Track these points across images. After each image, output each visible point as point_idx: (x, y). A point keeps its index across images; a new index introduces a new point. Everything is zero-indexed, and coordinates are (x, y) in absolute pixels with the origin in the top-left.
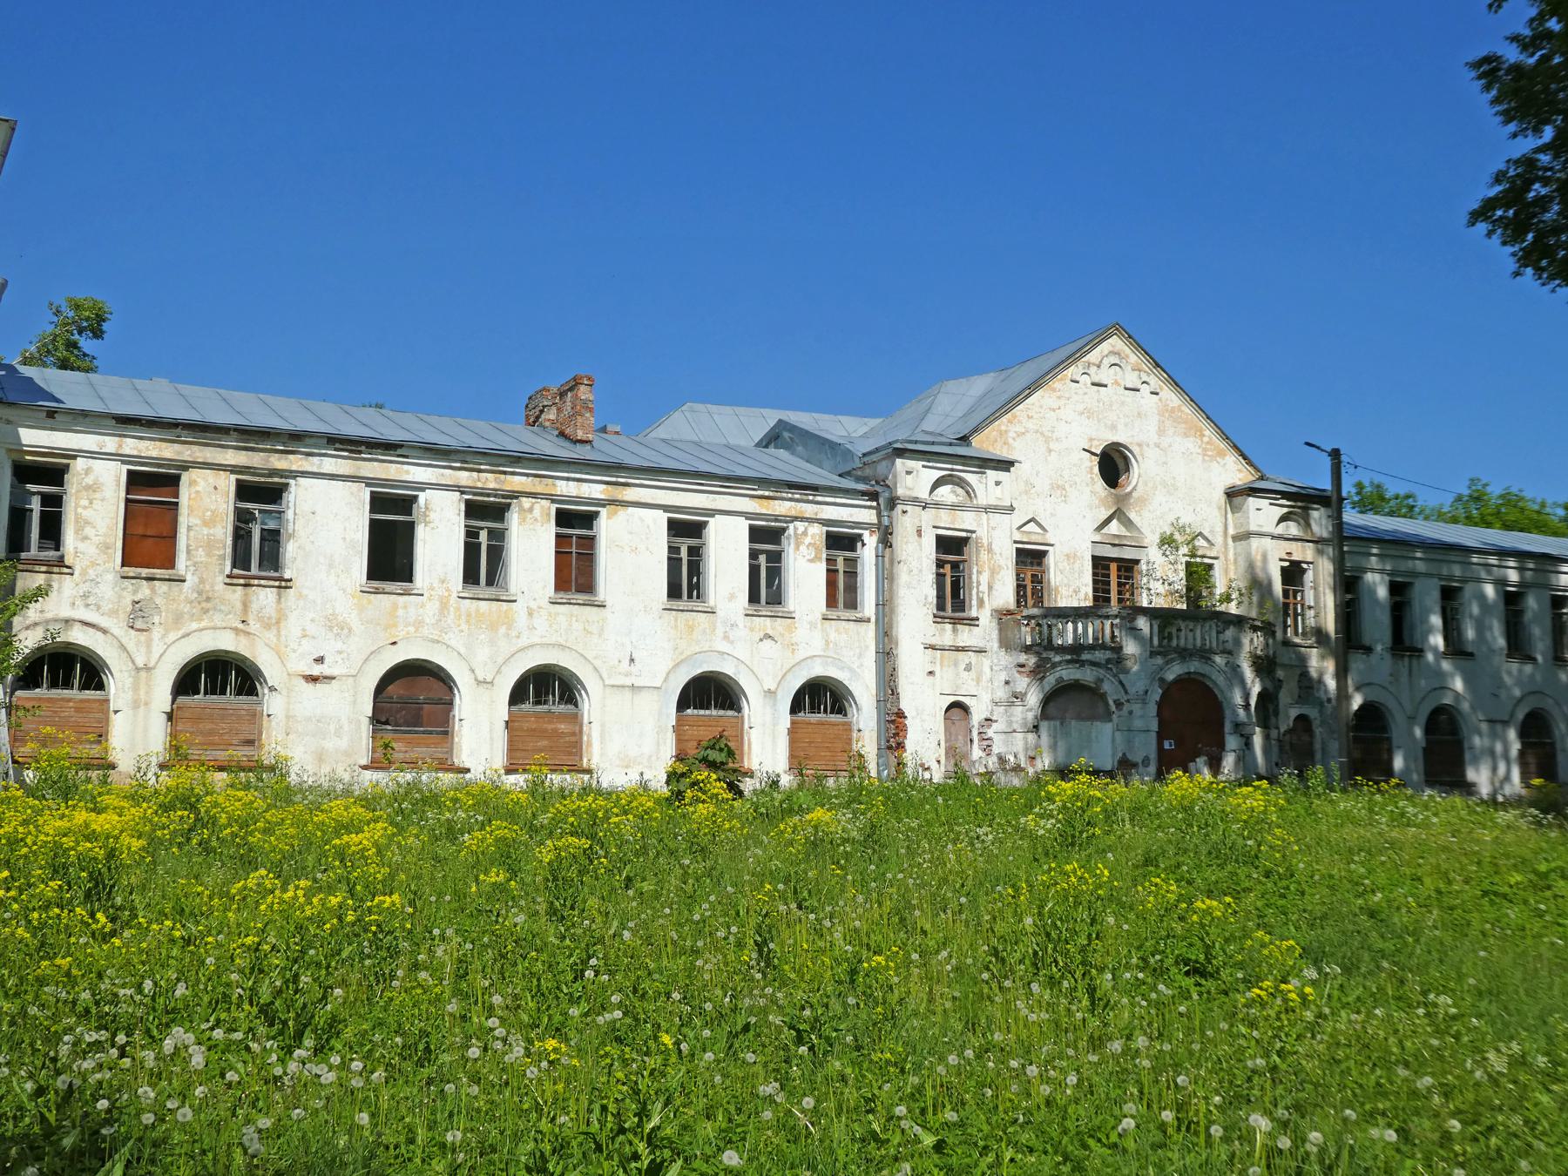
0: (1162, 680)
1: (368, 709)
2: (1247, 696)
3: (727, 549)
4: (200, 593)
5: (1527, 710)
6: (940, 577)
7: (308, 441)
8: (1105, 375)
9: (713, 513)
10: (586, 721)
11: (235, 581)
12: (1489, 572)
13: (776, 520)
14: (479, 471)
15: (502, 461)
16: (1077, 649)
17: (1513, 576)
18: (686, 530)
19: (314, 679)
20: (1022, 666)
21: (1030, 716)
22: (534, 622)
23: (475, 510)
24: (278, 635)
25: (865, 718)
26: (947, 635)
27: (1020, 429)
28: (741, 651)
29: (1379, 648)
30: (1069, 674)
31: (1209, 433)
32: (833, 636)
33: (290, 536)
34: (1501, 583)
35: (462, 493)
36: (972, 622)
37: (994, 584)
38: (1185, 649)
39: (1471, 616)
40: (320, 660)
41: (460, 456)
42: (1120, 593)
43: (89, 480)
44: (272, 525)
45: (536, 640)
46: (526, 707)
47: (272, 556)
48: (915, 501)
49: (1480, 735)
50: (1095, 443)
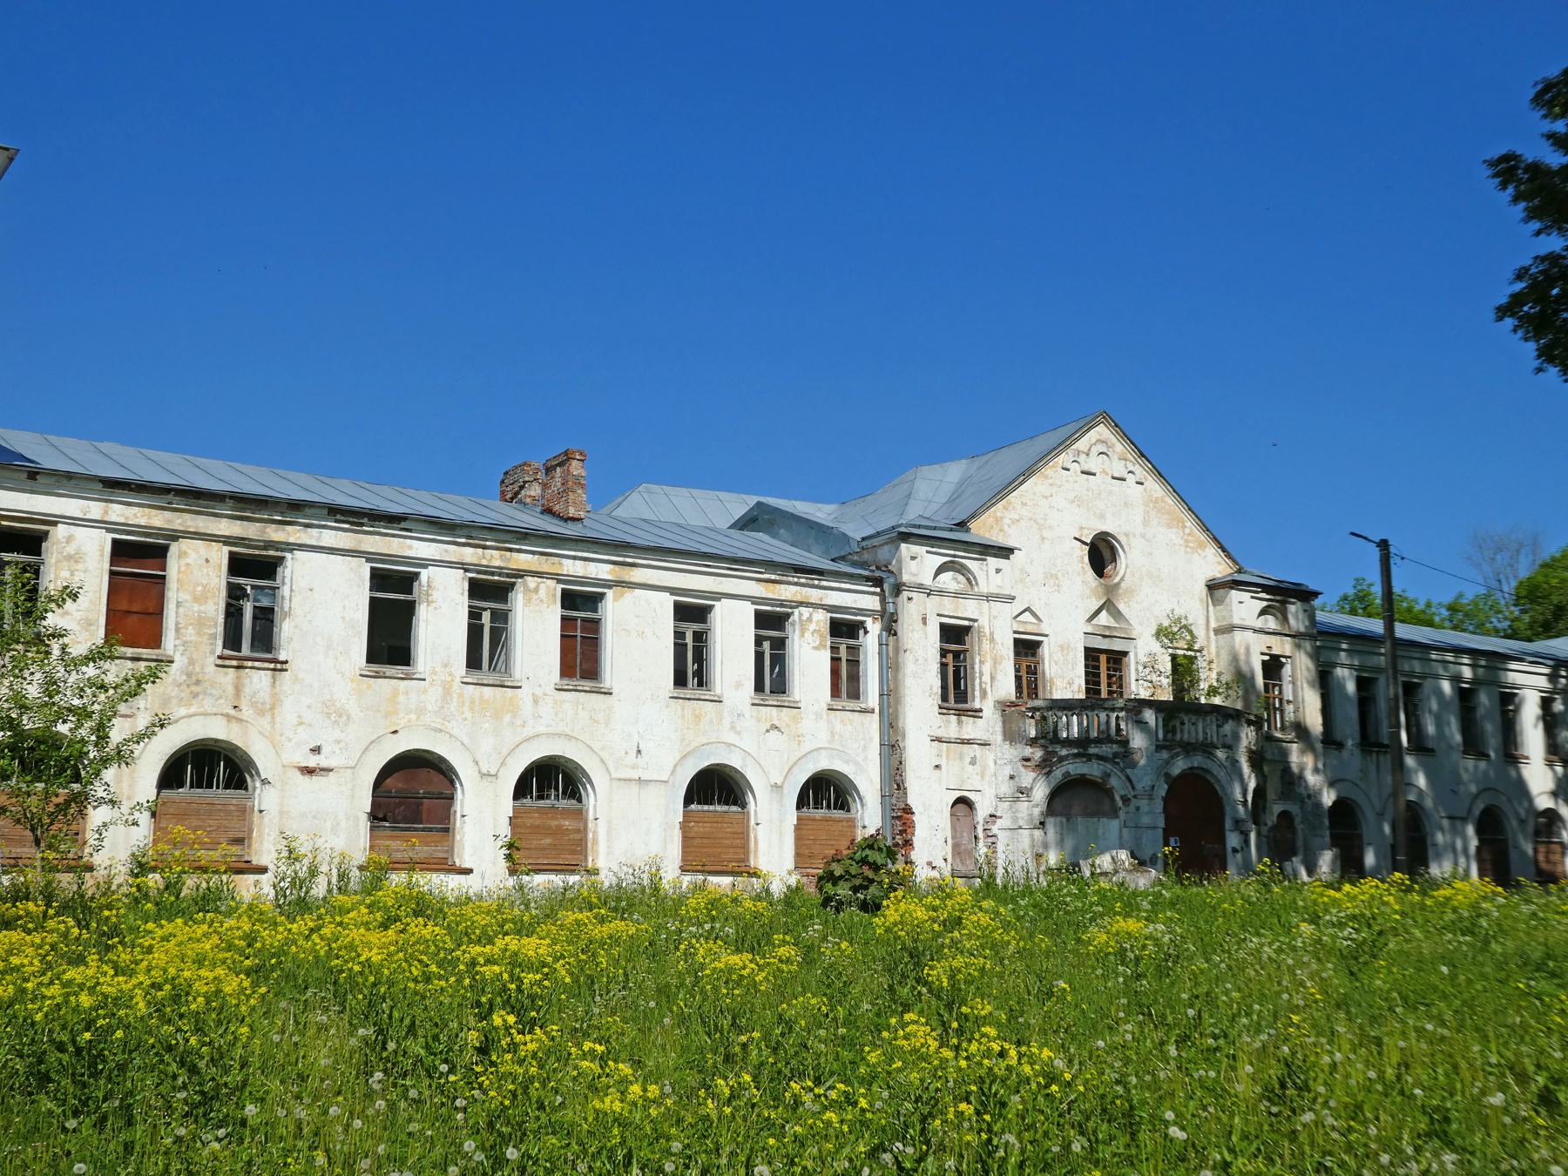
0: (1167, 775)
1: (366, 804)
2: (1245, 794)
3: (733, 634)
4: (189, 675)
5: (1482, 806)
6: (944, 666)
7: (308, 511)
8: (1093, 463)
9: (718, 596)
10: (591, 816)
11: (227, 662)
12: (1446, 669)
13: (782, 606)
14: (485, 547)
15: (508, 537)
16: (1083, 742)
17: (1467, 673)
18: (692, 614)
19: (309, 771)
20: (1027, 760)
21: (1037, 811)
22: (534, 712)
23: (479, 590)
24: (273, 722)
25: (869, 817)
26: (951, 726)
27: (1014, 516)
28: (747, 743)
29: (1350, 743)
30: (1076, 768)
31: (1190, 524)
32: (838, 727)
33: (286, 615)
34: (1456, 679)
35: (466, 570)
36: (976, 713)
37: (995, 676)
38: (1189, 744)
39: (1430, 711)
40: (316, 750)
41: (464, 532)
42: (1109, 685)
43: (71, 549)
44: (265, 603)
45: (542, 729)
46: (527, 801)
47: (265, 638)
48: (920, 587)
49: (1442, 829)
50: (1086, 532)
